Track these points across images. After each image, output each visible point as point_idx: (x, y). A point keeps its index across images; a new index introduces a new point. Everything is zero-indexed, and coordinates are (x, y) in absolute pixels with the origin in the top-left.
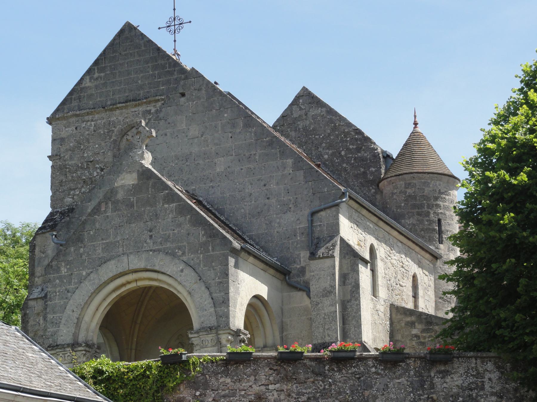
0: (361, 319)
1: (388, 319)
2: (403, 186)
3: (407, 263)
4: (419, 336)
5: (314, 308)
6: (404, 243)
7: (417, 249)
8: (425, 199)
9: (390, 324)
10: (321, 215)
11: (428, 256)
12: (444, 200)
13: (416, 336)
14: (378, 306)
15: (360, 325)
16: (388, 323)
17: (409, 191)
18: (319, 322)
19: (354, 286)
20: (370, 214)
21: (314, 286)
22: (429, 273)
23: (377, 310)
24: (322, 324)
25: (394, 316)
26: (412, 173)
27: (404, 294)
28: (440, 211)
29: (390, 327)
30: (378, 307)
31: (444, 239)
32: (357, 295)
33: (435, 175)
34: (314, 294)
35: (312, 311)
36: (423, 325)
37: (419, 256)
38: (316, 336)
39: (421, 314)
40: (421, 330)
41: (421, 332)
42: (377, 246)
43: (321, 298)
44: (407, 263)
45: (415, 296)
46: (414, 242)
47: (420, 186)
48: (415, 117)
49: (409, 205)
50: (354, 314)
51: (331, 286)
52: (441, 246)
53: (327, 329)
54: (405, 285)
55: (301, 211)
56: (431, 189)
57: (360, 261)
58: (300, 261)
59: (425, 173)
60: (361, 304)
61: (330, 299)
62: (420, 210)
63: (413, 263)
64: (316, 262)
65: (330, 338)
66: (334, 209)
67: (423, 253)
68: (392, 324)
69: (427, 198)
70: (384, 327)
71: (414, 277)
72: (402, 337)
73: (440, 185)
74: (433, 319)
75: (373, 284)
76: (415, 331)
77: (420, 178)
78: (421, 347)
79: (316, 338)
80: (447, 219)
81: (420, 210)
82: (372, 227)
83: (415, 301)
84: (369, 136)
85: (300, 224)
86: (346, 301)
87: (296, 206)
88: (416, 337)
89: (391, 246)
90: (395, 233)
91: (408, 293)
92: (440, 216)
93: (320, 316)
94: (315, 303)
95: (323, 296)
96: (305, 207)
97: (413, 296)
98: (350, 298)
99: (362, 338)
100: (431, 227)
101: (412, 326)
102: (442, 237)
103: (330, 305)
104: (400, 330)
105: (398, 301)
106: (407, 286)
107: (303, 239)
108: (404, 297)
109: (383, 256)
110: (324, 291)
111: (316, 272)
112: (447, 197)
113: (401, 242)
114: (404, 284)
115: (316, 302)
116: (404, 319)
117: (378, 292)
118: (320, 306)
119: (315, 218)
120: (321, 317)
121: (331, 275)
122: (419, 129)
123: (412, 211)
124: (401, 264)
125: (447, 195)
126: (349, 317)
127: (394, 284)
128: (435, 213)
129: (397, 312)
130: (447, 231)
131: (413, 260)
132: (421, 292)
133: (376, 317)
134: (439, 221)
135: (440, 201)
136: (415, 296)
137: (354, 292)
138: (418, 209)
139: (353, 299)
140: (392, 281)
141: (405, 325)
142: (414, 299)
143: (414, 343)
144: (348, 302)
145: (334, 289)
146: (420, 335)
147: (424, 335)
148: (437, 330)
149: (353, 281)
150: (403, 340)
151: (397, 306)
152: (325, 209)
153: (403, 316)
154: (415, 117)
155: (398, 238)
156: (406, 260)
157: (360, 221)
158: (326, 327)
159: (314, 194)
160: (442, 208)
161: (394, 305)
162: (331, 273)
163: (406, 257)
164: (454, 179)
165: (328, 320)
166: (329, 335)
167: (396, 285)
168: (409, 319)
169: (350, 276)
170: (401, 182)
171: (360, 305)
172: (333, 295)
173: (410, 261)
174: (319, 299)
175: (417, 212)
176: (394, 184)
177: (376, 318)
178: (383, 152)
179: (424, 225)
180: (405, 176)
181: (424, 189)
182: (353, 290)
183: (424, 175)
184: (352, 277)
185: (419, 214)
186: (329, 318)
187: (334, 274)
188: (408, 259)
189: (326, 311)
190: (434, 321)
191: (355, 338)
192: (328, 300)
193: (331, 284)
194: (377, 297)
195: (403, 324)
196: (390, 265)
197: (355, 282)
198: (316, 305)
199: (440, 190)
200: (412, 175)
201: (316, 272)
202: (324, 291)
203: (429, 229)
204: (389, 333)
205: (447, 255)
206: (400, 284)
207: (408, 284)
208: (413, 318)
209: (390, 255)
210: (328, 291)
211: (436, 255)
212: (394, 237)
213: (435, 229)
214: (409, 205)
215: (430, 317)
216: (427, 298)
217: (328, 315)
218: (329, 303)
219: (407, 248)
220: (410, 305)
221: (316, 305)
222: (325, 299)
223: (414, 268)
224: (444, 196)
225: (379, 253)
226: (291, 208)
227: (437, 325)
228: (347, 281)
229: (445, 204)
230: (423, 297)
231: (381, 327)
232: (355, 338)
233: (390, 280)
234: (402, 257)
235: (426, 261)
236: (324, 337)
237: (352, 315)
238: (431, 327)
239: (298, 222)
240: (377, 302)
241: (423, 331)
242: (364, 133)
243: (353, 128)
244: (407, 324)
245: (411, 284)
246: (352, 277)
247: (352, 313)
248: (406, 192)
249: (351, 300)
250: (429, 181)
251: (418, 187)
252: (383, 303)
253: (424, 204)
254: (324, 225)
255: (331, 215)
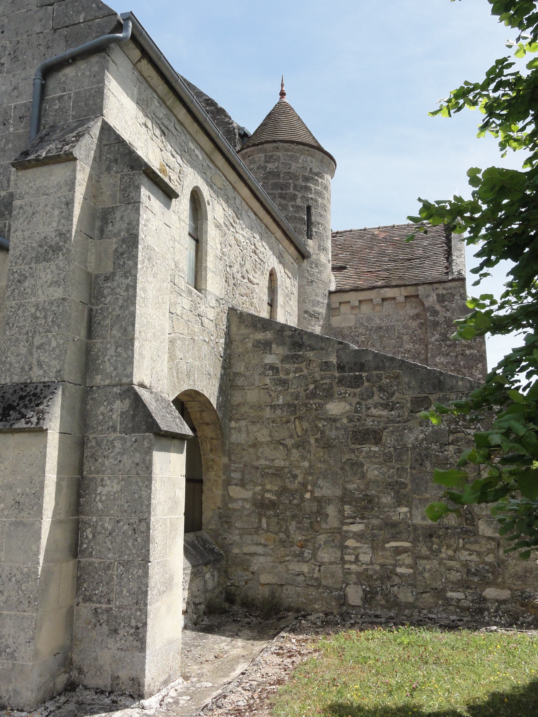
0: (133, 325)
1: (223, 335)
2: (263, 159)
3: (262, 250)
4: (277, 369)
5: (14, 290)
6: (260, 216)
7: (279, 234)
8: (291, 178)
9: (226, 344)
10: (65, 75)
11: (292, 249)
12: (316, 183)
13: (273, 368)
14: (203, 307)
15: (132, 341)
16: (222, 341)
17: (270, 166)
18: (20, 328)
19: (123, 241)
20: (196, 125)
21: (19, 233)
22: (292, 275)
23: (199, 315)
24: (27, 334)
25: (234, 329)
26: (275, 141)
27: (255, 297)
28: (310, 196)
29: (225, 350)
30: (202, 309)
31: (314, 234)
32: (130, 263)
33: (306, 148)
34: (18, 254)
35: (8, 297)
36: (286, 349)
37: (281, 246)
38: (11, 364)
39: (284, 327)
40: (281, 358)
41: (282, 361)
42: (209, 198)
43: (33, 265)
44: (262, 250)
45: (272, 304)
46: (275, 220)
47: (285, 160)
48: (282, 85)
49: (270, 183)
50: (118, 311)
51: (61, 234)
52: (310, 242)
53: (38, 348)
54: (258, 282)
55: (24, 68)
56: (300, 165)
57: (145, 179)
58: (9, 181)
59: (292, 142)
60: (139, 286)
61: (53, 268)
62: (284, 192)
63: (271, 253)
64: (30, 173)
65: (41, 372)
66: (94, 59)
67: (286, 243)
68: (229, 343)
69: (295, 177)
70: (213, 348)
71: (272, 274)
72: (247, 368)
73: (312, 162)
74: (305, 337)
75: (196, 266)
76: (270, 359)
77: (287, 150)
78: (280, 388)
79: (9, 370)
80: (319, 208)
81: (284, 192)
82: (200, 157)
83: (271, 312)
84: (223, 107)
85: (17, 97)
86: (102, 278)
87: (15, 59)
88: (272, 371)
89: (238, 214)
90: (246, 192)
91: (262, 295)
92: (311, 203)
93: (24, 312)
94: (16, 275)
95: (37, 260)
96: (34, 59)
97: (268, 304)
98: (112, 270)
99: (132, 374)
100: (297, 215)
101: (265, 349)
102: (311, 231)
103: (51, 284)
104: (244, 356)
105: (244, 306)
106: (261, 284)
107: (21, 131)
108: (255, 301)
109: (221, 221)
110: (41, 246)
111: (27, 199)
112: (320, 180)
113: (255, 214)
114: (256, 281)
115: (21, 275)
116: (251, 336)
117: (206, 280)
118: (26, 284)
119: (52, 83)
120: (26, 314)
121: (63, 206)
122: (286, 99)
123: (274, 192)
124: (253, 247)
125: (320, 177)
126: (104, 318)
127: (239, 276)
128: (303, 197)
129: (240, 322)
130: (319, 224)
131: (271, 248)
132: (280, 299)
133: (197, 328)
134: (309, 208)
135: (312, 183)
136: (272, 304)
137: (122, 254)
138: (282, 189)
139: (119, 273)
140: (235, 269)
141: (253, 346)
142: (269, 307)
143: (267, 381)
144: (107, 279)
145: (65, 242)
146: (279, 365)
147: (287, 366)
148: (312, 358)
149: (124, 226)
150: (248, 374)
151: (241, 313)
152: (74, 59)
153: (250, 330)
154: (282, 85)
155: (249, 203)
156: (260, 244)
157: (174, 131)
158: (37, 341)
159: (55, 30)
160: (313, 192)
161: (236, 310)
162: (64, 200)
163: (261, 239)
164: (329, 159)
165: (43, 322)
166: (40, 364)
167: (242, 279)
168: (260, 336)
169: (118, 215)
170: (260, 155)
171: (135, 288)
172: (61, 257)
173: (267, 247)
174: (27, 268)
175: (280, 194)
176: (250, 158)
177: (196, 330)
178: (240, 128)
179: (288, 212)
180: (267, 146)
181: (290, 164)
182: (121, 250)
183: (293, 146)
184: (122, 218)
185: (282, 196)
186: (45, 317)
187: (69, 204)
188: (264, 244)
189: (41, 299)
190: (306, 341)
191: (114, 374)
192: (48, 271)
193: (61, 227)
194: (203, 291)
195: (250, 345)
196: (233, 242)
197: (128, 230)
198: (19, 281)
199: (311, 169)
200: (275, 144)
201: (27, 199)
202: (41, 246)
203: (296, 218)
204: (222, 359)
205: (317, 254)
206: (248, 278)
207: (264, 282)
208: (269, 335)
209: (235, 225)
210: (51, 247)
211: (303, 250)
212: (243, 199)
213: (304, 219)
214: (270, 183)
215: (299, 334)
216: (288, 309)
217: (44, 308)
218: (49, 276)
219: (263, 226)
220: (264, 314)
221: (19, 281)
222: (40, 266)
223: (272, 262)
224: (316, 177)
225: (213, 212)
226: (4, 64)
227: (312, 349)
228: (110, 227)
229: (317, 188)
230: (283, 307)
231: (205, 349)
232: (114, 374)
233: (230, 266)
234: (254, 237)
235: (289, 257)
236: (27, 368)
237: (114, 313)
238: (301, 353)
239: (15, 93)
240: (201, 298)
241: (285, 359)
242: (217, 104)
243: (205, 97)
244: (258, 344)
245: (267, 283)
246: (122, 218)
247: (113, 310)
248: (266, 167)
249: (114, 274)
250: (298, 155)
251: (282, 161)
252: (213, 303)
253: (290, 184)
254: (70, 98)
255: (88, 73)
